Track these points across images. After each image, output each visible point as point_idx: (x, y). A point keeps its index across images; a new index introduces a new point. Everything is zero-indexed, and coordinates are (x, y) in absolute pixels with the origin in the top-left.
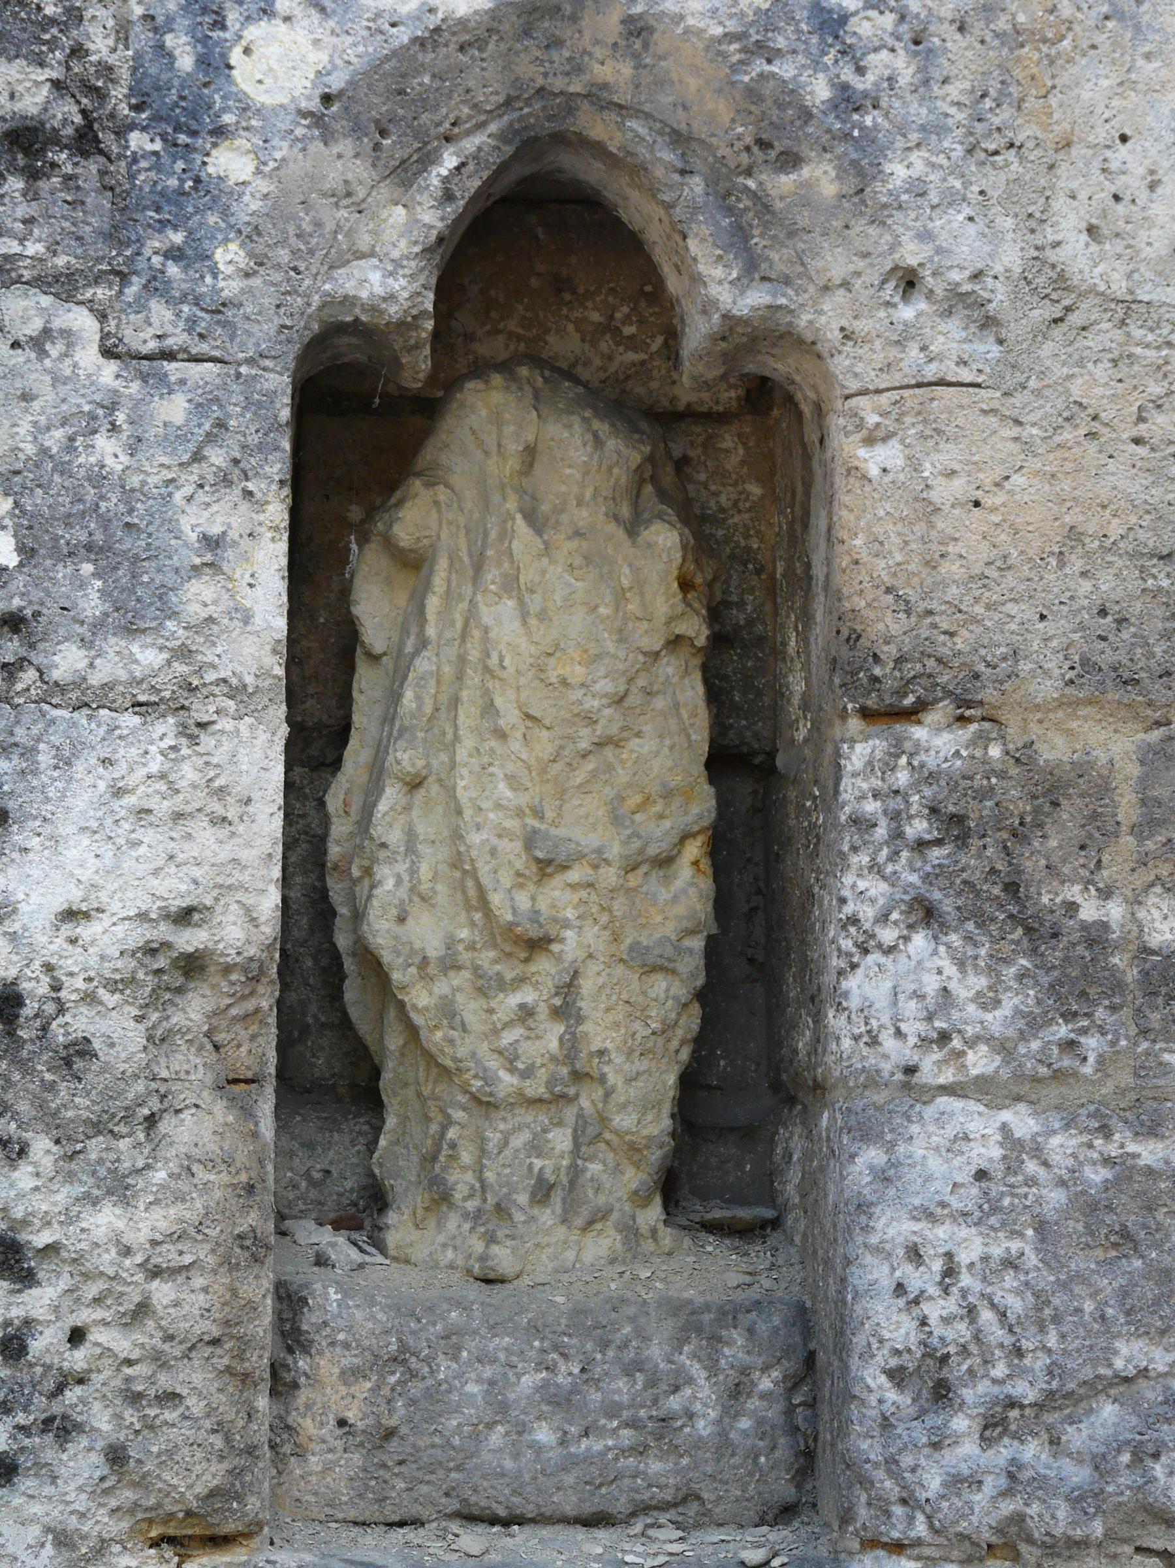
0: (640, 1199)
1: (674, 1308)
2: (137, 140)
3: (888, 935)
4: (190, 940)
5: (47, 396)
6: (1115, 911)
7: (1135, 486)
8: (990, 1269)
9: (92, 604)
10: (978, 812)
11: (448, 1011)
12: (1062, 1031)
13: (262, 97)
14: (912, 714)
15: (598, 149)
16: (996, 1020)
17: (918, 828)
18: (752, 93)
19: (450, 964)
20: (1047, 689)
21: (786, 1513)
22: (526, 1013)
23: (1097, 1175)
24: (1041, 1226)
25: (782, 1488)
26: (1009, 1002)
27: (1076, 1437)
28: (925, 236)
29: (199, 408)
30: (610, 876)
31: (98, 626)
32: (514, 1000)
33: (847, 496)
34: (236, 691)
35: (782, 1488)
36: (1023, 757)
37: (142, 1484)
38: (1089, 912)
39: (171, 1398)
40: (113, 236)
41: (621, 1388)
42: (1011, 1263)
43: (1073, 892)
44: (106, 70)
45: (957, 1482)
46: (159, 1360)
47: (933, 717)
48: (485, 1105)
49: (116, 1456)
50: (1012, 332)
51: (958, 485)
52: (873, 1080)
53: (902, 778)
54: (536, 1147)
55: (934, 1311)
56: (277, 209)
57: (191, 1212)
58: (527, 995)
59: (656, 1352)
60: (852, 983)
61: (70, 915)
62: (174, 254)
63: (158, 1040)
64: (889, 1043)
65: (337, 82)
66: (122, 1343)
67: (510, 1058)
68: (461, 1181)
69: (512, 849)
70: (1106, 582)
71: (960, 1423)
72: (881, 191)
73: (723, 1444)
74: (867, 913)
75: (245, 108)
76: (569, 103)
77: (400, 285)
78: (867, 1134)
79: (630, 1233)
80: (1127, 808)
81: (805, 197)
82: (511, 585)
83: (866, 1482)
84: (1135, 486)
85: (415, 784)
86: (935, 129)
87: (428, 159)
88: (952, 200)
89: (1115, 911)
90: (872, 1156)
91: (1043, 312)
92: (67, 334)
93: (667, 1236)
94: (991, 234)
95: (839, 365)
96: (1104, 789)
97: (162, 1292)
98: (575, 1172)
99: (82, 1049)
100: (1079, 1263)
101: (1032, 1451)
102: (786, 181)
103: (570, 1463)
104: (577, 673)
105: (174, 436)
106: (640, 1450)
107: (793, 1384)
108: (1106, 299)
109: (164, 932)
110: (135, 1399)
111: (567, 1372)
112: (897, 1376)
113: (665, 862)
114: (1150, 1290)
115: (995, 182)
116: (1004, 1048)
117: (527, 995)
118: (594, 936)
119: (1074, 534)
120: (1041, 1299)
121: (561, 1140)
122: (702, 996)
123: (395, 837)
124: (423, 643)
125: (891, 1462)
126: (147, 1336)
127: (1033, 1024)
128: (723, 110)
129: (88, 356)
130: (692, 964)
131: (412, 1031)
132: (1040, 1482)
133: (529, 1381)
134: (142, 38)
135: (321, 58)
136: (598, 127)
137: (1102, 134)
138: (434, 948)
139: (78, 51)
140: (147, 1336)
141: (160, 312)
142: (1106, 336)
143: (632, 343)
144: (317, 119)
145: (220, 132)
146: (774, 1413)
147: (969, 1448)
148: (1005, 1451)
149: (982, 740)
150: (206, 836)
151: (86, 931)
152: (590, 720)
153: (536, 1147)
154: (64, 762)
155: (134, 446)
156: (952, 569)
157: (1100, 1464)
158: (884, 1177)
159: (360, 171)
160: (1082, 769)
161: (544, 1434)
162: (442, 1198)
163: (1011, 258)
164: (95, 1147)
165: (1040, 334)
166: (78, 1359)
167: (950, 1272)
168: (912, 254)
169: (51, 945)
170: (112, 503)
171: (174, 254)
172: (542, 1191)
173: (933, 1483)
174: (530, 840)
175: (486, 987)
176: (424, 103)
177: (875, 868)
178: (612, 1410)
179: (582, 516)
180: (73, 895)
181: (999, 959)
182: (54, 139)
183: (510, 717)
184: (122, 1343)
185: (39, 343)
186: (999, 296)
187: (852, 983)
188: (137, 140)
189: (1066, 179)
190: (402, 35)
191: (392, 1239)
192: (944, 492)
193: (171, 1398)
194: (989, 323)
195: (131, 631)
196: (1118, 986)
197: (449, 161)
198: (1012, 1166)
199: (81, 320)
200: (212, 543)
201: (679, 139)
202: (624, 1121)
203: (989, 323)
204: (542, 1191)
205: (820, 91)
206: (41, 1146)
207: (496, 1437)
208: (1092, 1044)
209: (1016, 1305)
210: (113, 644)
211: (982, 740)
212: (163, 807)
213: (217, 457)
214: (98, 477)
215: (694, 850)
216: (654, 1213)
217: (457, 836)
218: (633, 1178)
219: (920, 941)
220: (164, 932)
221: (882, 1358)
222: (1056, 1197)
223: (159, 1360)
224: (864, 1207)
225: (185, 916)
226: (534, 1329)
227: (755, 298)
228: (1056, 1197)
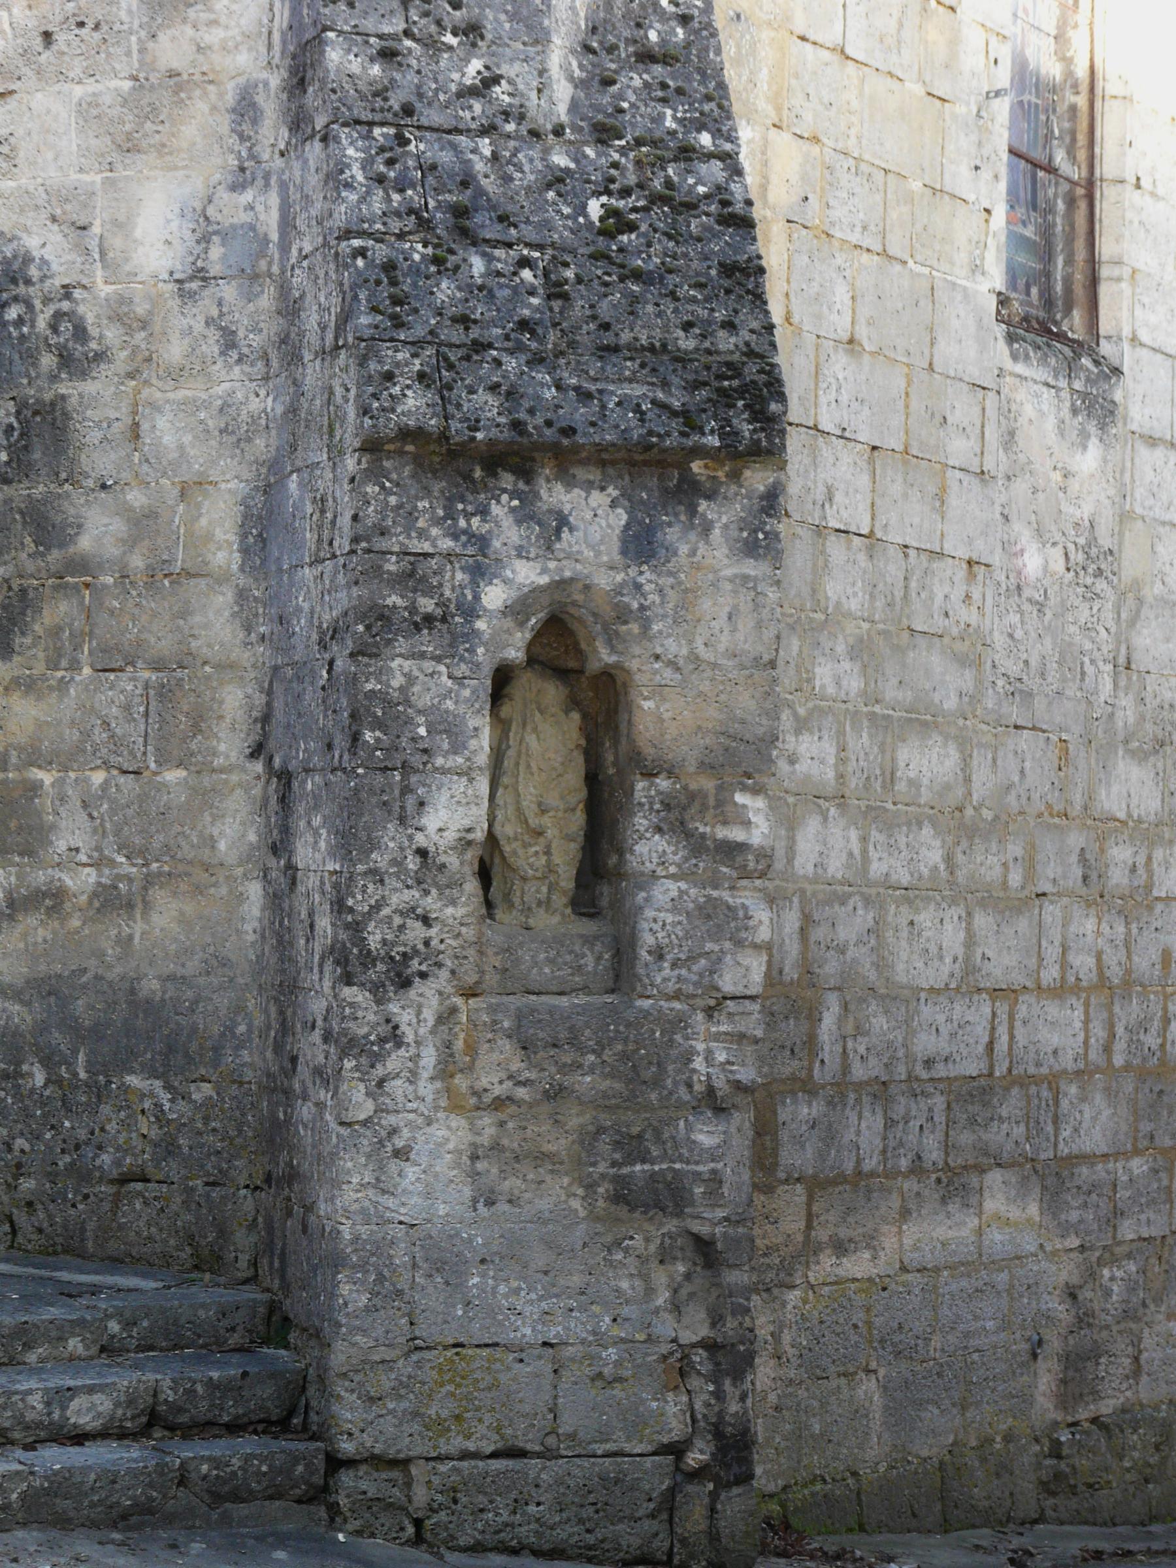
0: (566, 906)
1: (582, 936)
2: (457, 619)
3: (648, 835)
4: (470, 836)
5: (434, 689)
6: (708, 829)
7: (716, 714)
8: (674, 924)
9: (446, 746)
10: (673, 803)
11: (515, 853)
12: (694, 861)
13: (489, 607)
14: (656, 775)
15: (572, 616)
16: (677, 858)
17: (657, 806)
18: (617, 605)
19: (516, 839)
20: (692, 769)
21: (613, 991)
22: (537, 853)
23: (702, 900)
24: (688, 913)
25: (611, 984)
26: (681, 854)
27: (695, 968)
28: (662, 645)
29: (473, 692)
30: (560, 814)
31: (447, 752)
32: (533, 849)
33: (637, 718)
34: (480, 769)
35: (611, 984)
36: (685, 788)
37: (459, 980)
38: (701, 830)
39: (466, 957)
40: (451, 645)
41: (568, 958)
42: (680, 923)
43: (697, 824)
44: (449, 600)
45: (665, 980)
46: (463, 947)
47: (661, 776)
48: (524, 879)
49: (453, 972)
50: (685, 671)
51: (670, 714)
52: (642, 874)
53: (653, 793)
54: (538, 891)
55: (660, 935)
56: (493, 636)
57: (470, 909)
58: (537, 848)
59: (577, 948)
60: (636, 848)
61: (440, 830)
62: (466, 650)
63: (462, 863)
64: (648, 864)
65: (509, 603)
66: (454, 943)
67: (531, 866)
68: (517, 901)
69: (534, 807)
70: (708, 741)
71: (666, 965)
72: (651, 633)
73: (595, 973)
74: (642, 829)
75: (485, 610)
76: (566, 605)
77: (520, 654)
78: (642, 889)
79: (563, 915)
80: (711, 801)
81: (629, 632)
82: (535, 730)
83: (640, 980)
84: (716, 714)
85: (506, 787)
86: (664, 616)
87: (528, 619)
88: (669, 635)
89: (708, 829)
90: (643, 894)
91: (692, 667)
92: (439, 673)
93: (573, 917)
94: (680, 645)
95: (637, 677)
96: (706, 796)
97: (464, 930)
98: (549, 899)
99: (443, 866)
100: (697, 923)
101: (684, 972)
102: (624, 628)
103: (554, 978)
104: (553, 756)
105: (467, 700)
106: (572, 975)
107: (613, 956)
108: (709, 663)
109: (463, 834)
110: (457, 957)
111: (553, 953)
112: (649, 952)
113: (573, 810)
114: (714, 930)
115: (680, 631)
116: (679, 866)
117: (537, 848)
118: (556, 832)
119: (700, 728)
120: (687, 932)
121: (544, 889)
122: (583, 848)
123: (501, 803)
124: (509, 747)
125: (648, 975)
126: (460, 941)
127: (686, 859)
128: (608, 609)
129: (444, 678)
130: (581, 839)
131: (504, 858)
132: (686, 980)
133: (542, 956)
134: (458, 590)
135: (505, 596)
136: (572, 610)
137: (708, 617)
138: (511, 834)
139: (442, 595)
140: (460, 941)
141: (463, 666)
142: (709, 673)
143: (556, 649)
144: (503, 613)
145: (478, 617)
146: (608, 964)
147: (668, 971)
148: (676, 972)
149: (674, 783)
150: (474, 808)
151: (445, 834)
152: (555, 769)
153: (538, 891)
154: (439, 789)
155: (456, 703)
156: (668, 737)
157: (701, 975)
158: (647, 900)
159: (512, 624)
160: (700, 791)
161: (547, 970)
162: (511, 905)
163: (684, 651)
164: (447, 891)
165: (692, 672)
166: (442, 947)
167: (664, 925)
168: (659, 650)
169: (436, 838)
170: (450, 719)
171: (466, 650)
172: (540, 903)
173: (659, 980)
174: (540, 804)
175: (525, 846)
176: (529, 606)
177: (645, 817)
178: (566, 964)
179: (553, 710)
180: (441, 825)
181: (678, 842)
182: (436, 619)
183: (535, 769)
184: (454, 943)
185: (432, 675)
186: (681, 662)
187: (636, 848)
188: (457, 619)
189: (699, 630)
190: (526, 590)
191: (497, 917)
192: (666, 716)
193: (466, 957)
194: (678, 669)
195: (455, 753)
196: (708, 850)
197: (533, 620)
198: (680, 897)
199: (443, 668)
200: (476, 729)
201: (594, 614)
202: (563, 884)
203: (678, 669)
204: (540, 903)
205: (635, 605)
206: (434, 891)
207: (535, 971)
208: (701, 865)
209: (680, 934)
210: (451, 757)
211: (674, 783)
212: (464, 801)
213: (477, 706)
214: (447, 711)
215: (581, 806)
216: (569, 911)
217: (518, 802)
218: (564, 900)
219: (657, 837)
220: (463, 834)
221: (646, 948)
222: (691, 905)
223: (463, 947)
224: (641, 908)
225: (469, 830)
226: (543, 942)
227: (613, 659)
228: (691, 905)
